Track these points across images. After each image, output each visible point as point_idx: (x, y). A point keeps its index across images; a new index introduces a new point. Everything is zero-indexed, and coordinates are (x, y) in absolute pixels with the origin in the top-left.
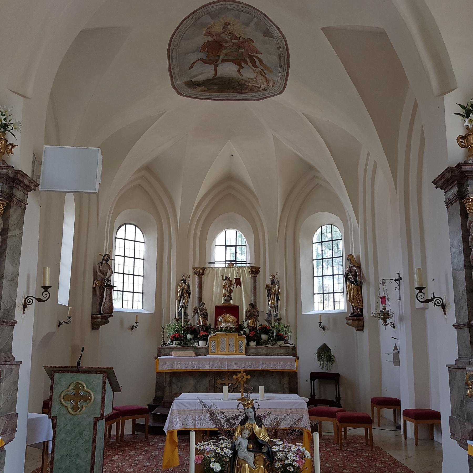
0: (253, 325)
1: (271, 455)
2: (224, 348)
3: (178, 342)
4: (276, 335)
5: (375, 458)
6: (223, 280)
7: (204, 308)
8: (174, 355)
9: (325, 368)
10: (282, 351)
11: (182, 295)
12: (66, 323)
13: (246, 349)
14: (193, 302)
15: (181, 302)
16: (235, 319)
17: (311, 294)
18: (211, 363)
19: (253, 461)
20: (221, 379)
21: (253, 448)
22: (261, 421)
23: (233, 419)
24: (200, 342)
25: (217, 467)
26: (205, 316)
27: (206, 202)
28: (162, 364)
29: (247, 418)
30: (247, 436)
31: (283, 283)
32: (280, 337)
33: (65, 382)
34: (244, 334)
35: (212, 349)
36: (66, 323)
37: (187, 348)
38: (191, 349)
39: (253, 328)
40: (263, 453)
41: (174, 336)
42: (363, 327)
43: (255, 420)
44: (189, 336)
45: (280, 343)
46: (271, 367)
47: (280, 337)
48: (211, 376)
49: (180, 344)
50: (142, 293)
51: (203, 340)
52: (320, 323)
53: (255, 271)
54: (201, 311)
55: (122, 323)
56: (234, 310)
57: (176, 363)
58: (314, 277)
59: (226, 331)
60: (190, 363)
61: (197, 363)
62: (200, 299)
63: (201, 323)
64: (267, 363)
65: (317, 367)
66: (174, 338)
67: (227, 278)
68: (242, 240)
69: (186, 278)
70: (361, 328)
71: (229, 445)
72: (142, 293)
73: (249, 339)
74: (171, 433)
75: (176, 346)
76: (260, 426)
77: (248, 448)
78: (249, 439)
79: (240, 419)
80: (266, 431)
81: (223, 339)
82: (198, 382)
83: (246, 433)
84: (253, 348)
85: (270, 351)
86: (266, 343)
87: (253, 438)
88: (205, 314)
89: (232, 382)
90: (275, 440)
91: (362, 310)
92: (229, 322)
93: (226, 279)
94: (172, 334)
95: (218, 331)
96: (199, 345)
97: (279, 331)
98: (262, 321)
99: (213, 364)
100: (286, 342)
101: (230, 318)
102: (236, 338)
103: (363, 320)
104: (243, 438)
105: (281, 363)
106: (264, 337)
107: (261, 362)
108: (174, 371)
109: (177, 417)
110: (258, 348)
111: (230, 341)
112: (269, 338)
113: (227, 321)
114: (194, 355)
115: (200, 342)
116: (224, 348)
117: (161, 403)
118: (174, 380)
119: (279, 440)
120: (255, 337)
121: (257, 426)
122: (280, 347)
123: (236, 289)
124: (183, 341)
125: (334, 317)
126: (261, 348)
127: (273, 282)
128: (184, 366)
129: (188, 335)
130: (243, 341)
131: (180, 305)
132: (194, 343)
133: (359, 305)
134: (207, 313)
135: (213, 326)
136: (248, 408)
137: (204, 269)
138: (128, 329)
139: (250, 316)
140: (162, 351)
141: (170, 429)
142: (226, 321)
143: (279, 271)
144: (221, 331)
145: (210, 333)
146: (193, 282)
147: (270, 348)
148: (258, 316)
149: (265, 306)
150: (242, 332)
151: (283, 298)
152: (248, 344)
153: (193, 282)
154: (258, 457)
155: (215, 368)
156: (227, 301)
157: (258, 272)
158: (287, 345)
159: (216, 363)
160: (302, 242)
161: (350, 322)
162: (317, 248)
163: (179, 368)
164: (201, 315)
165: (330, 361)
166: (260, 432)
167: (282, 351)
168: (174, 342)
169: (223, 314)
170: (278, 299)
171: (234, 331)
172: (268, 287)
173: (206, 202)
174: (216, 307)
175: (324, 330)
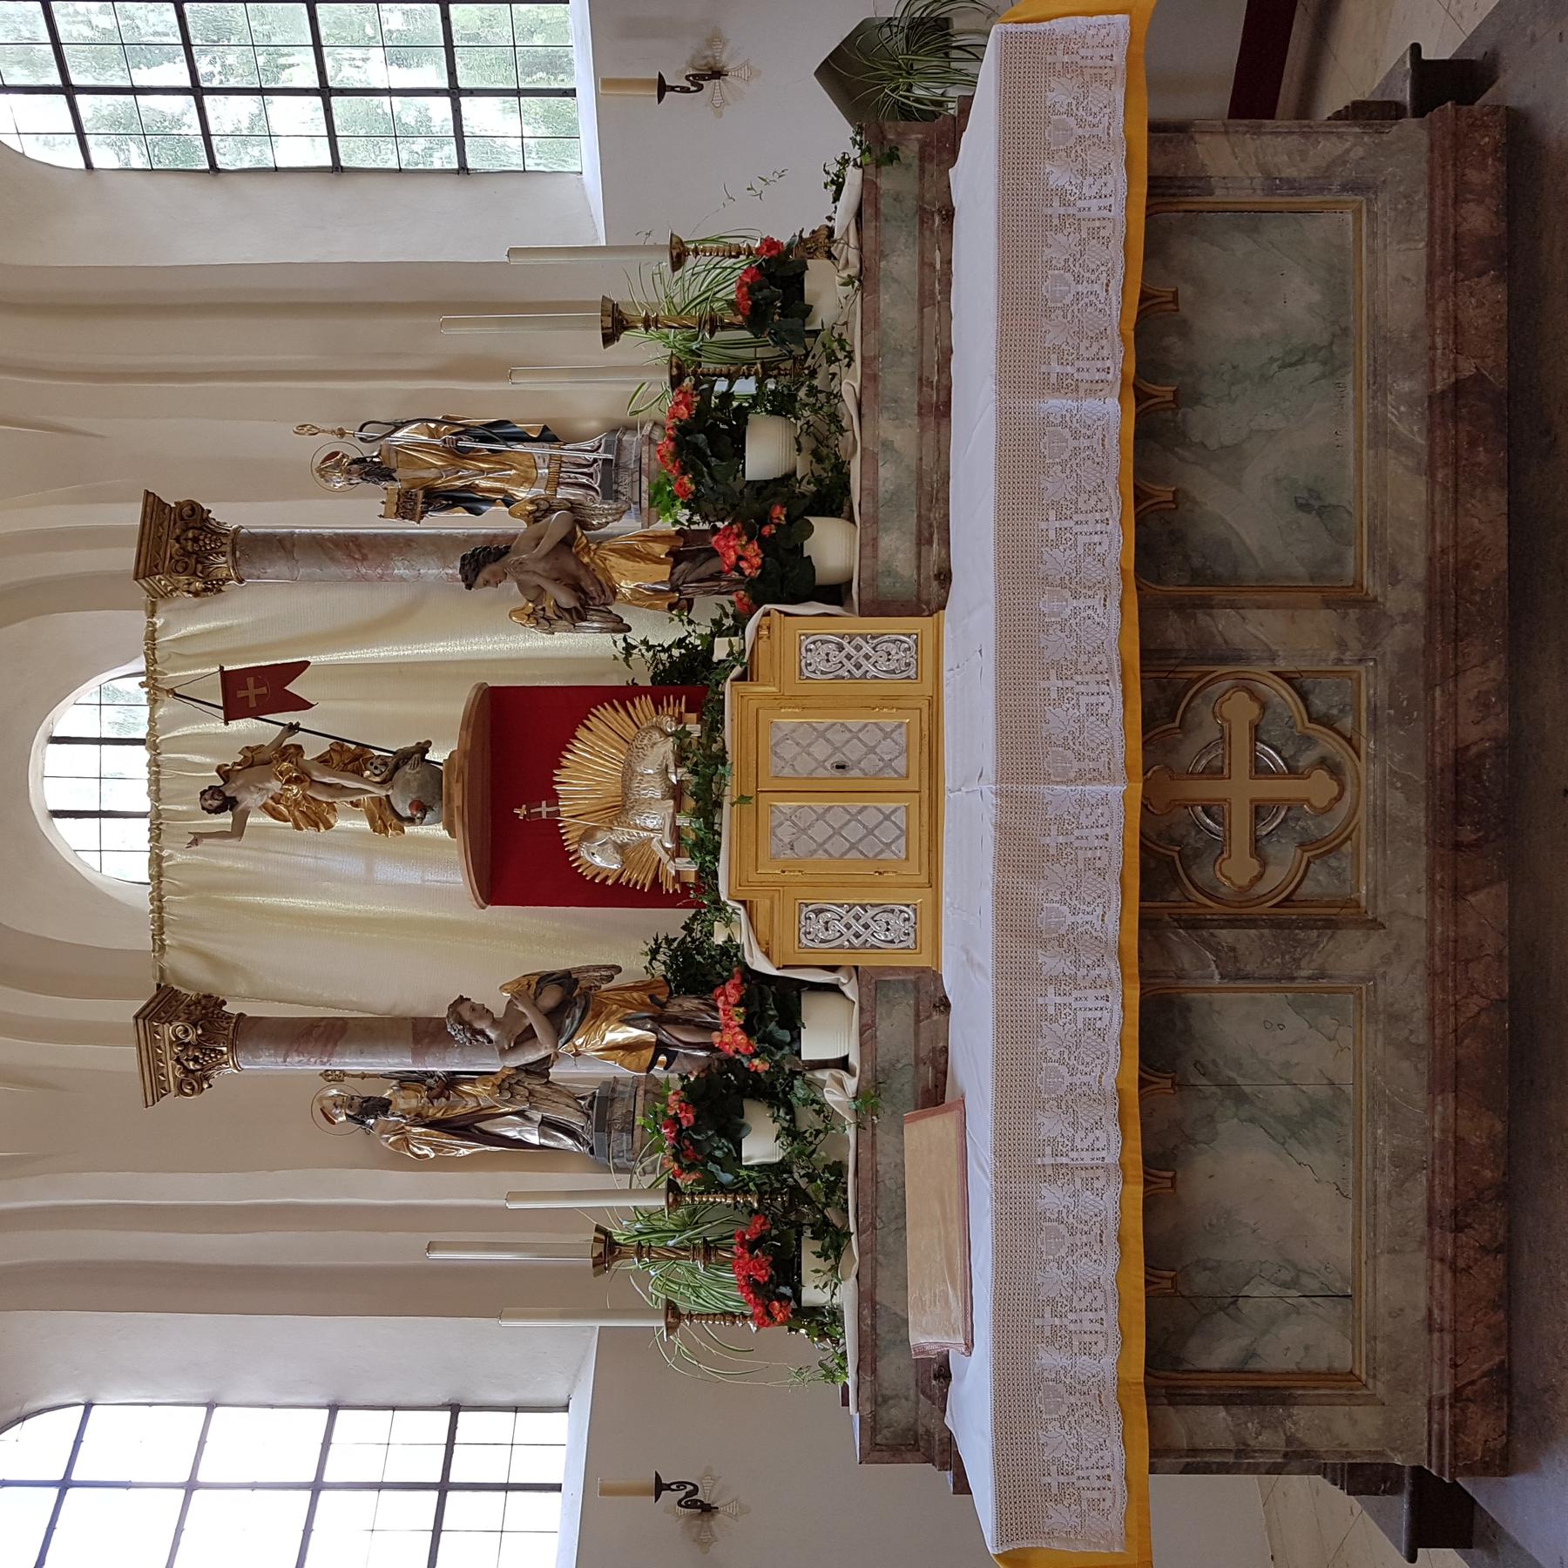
0: (660, 550)
2: (870, 818)
3: (809, 1262)
6: (238, 829)
7: (498, 1003)
10: (901, 264)
13: (879, 607)
15: (512, 1133)
16: (605, 720)
17: (454, 194)
18: (1053, 962)
20: (1218, 847)
24: (808, 1053)
26: (567, 999)
28: (1060, 1516)
31: (382, 397)
34: (738, 629)
35: (886, 938)
37: (872, 1180)
38: (883, 1138)
44: (761, 1145)
45: (827, 290)
48: (1186, 959)
49: (834, 1242)
50: (455, 1409)
51: (792, 1022)
52: (662, 88)
54: (527, 1037)
56: (519, 732)
58: (337, 168)
59: (708, 807)
60: (1052, 1197)
61: (1050, 1125)
63: (633, 1033)
64: (1054, 337)
66: (775, 1288)
67: (220, 799)
69: (349, 1102)
72: (455, 1409)
73: (788, 579)
81: (786, 833)
82: (1240, 1098)
84: (869, 545)
85: (899, 381)
86: (822, 445)
88: (550, 998)
89: (1241, 737)
92: (628, 773)
93: (228, 804)
95: (708, 875)
96: (843, 1064)
99: (1068, 942)
100: (822, 243)
101: (586, 772)
102: (780, 701)
105: (1058, 176)
106: (767, 451)
110: (870, 492)
111: (804, 766)
112: (782, 406)
113: (616, 793)
115: (808, 1053)
116: (870, 818)
117: (671, 735)
118: (1218, 1352)
120: (764, 519)
122: (864, 280)
123: (328, 716)
126: (870, 460)
127: (374, 471)
128: (1087, 1269)
130: (801, 636)
131: (534, 1139)
132: (822, 1109)
134: (545, 979)
135: (671, 921)
137: (165, 1003)
138: (704, 1543)
139: (576, 587)
140: (897, 1415)
142: (621, 808)
144: (706, 847)
145: (730, 952)
147: (870, 378)
150: (721, 650)
151: (483, 401)
152: (836, 593)
155: (1105, 911)
157: (193, 518)
159: (1057, 912)
167: (901, 264)
168: (812, 1295)
169: (552, 827)
170: (498, 432)
171: (714, 727)
175: (717, 74)
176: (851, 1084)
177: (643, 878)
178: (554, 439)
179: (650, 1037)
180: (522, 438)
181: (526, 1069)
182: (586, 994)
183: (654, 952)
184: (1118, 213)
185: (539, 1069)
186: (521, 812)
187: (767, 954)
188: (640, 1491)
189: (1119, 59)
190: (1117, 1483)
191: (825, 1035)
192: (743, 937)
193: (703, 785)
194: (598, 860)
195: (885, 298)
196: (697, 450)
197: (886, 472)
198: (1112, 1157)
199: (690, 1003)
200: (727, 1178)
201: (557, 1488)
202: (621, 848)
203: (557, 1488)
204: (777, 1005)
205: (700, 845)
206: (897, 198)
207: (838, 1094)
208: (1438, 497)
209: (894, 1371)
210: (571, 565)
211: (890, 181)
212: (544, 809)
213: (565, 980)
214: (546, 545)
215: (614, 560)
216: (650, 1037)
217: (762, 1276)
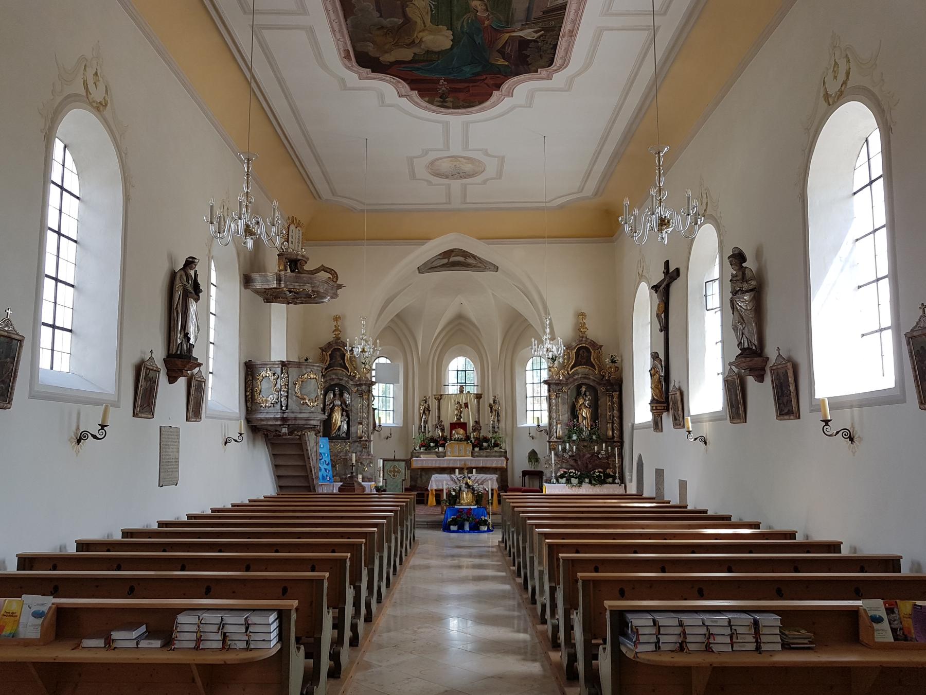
1: (473, 489)
8: (423, 457)
11: (424, 412)
12: (236, 441)
14: (432, 419)
25: (454, 493)
27: (442, 336)
31: (503, 402)
33: (389, 464)
35: (448, 453)
36: (236, 441)
39: (477, 439)
44: (432, 444)
45: (496, 449)
46: (488, 465)
47: (496, 445)
53: (478, 397)
56: (464, 426)
62: (439, 417)
65: (528, 467)
68: (471, 366)
73: (474, 446)
86: (486, 449)
87: (467, 484)
98: (484, 433)
101: (461, 431)
106: (485, 444)
107: (482, 462)
113: (459, 433)
123: (465, 411)
127: (494, 402)
129: (432, 444)
130: (470, 448)
143: (500, 393)
146: (433, 404)
149: (488, 420)
151: (503, 415)
153: (433, 404)
156: (459, 419)
160: (518, 369)
162: (529, 374)
170: (498, 415)
172: (490, 405)
173: (442, 336)
174: (451, 424)
191: (441, 449)
193: (459, 440)
201: (52, 368)
203: (52, 368)
208: (490, 549)
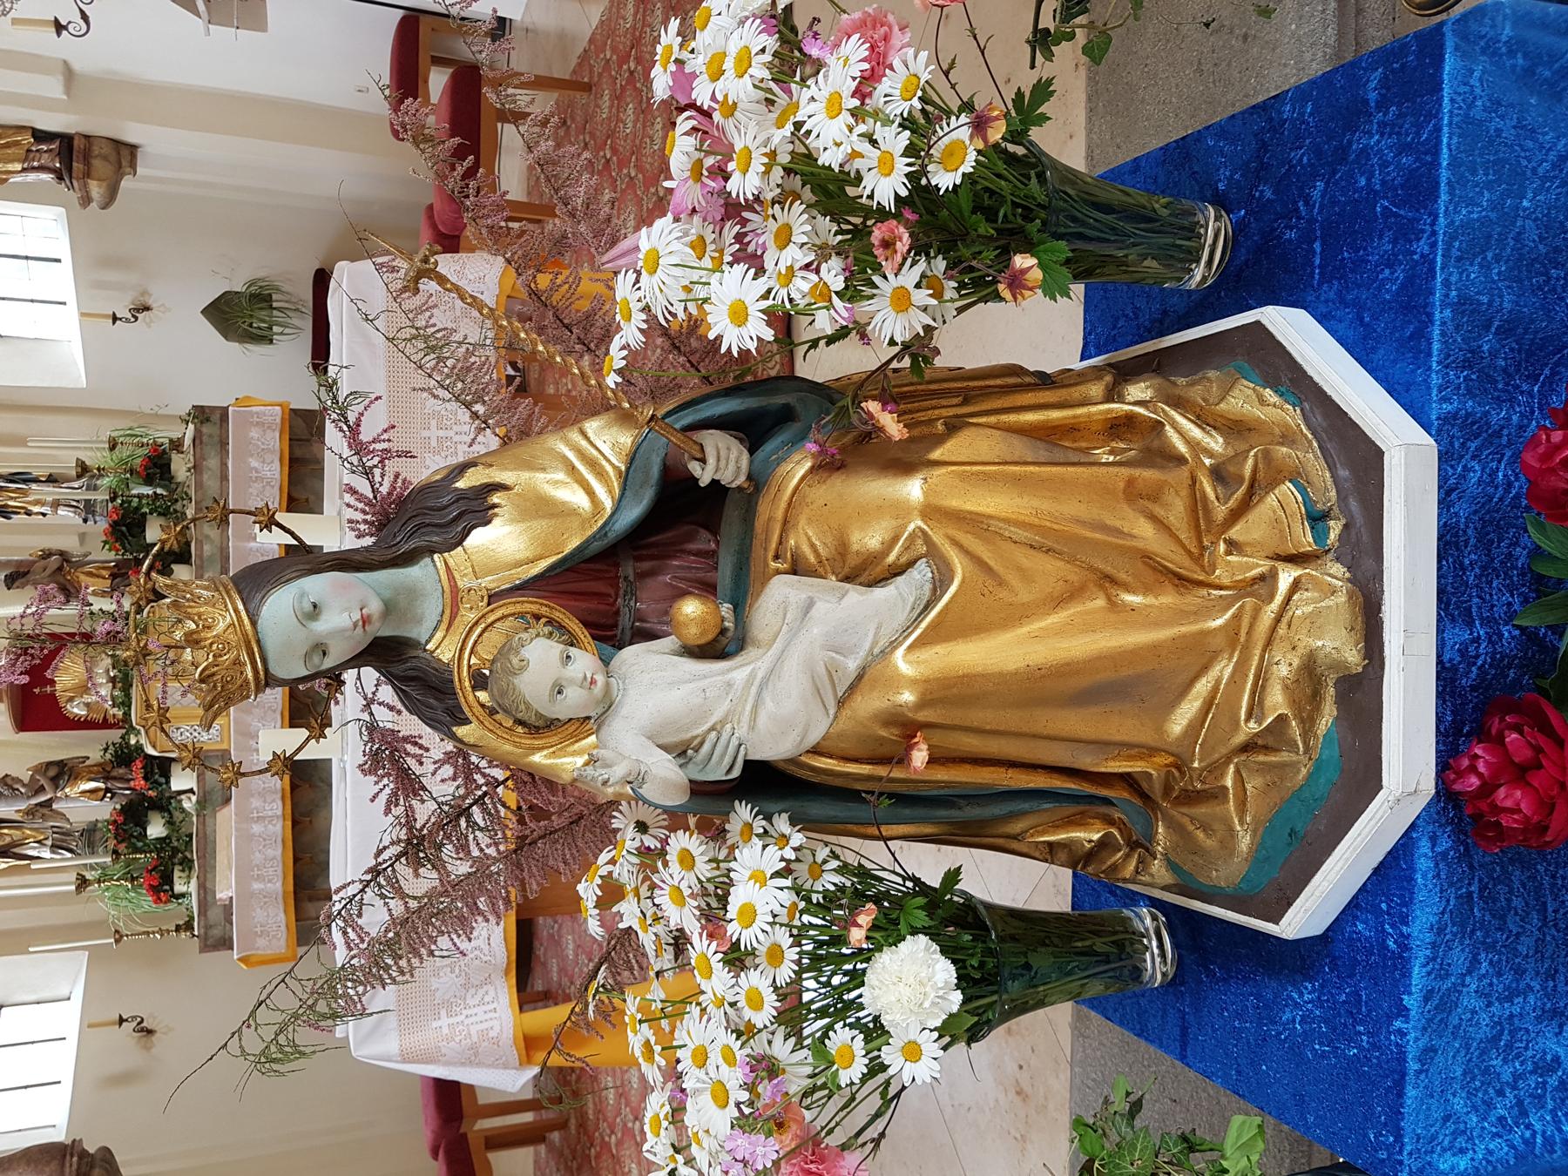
0: (106, 573)
3: (177, 874)
4: (149, 481)
5: (624, 59)
7: (26, 776)
9: (295, 321)
19: (855, 596)
21: (707, 589)
22: (427, 489)
23: (409, 785)
26: (62, 772)
29: (387, 652)
30: (584, 661)
32: (157, 466)
40: (757, 482)
41: (155, 891)
42: (117, 144)
43: (408, 559)
45: (180, 467)
47: (157, 466)
49: (187, 864)
51: (167, 775)
52: (115, 319)
54: (41, 789)
55: (123, 1079)
57: (256, 886)
59: (126, 689)
60: (257, 828)
66: (162, 887)
70: (124, 154)
71: (687, 860)
74: (530, 1044)
75: (194, 881)
76: (477, 508)
77: (717, 647)
78: (610, 634)
79: (410, 724)
80: (524, 450)
83: (549, 666)
87: (599, 591)
88: (52, 772)
90: (630, 334)
91: (40, 136)
94: (147, 902)
95: (127, 715)
96: (191, 791)
97: (132, 471)
100: (177, 445)
103: (87, 137)
104: (608, 705)
105: (254, 463)
106: (154, 532)
108: (291, 888)
109: (444, 1021)
110: (200, 556)
114: (225, 810)
119: (623, 286)
121: (478, 538)
122: (196, 468)
124: (175, 851)
125: (94, 262)
126: (200, 544)
128: (270, 852)
132: (183, 810)
133: (17, 143)
135: (115, 735)
136: (254, 644)
138: (148, 1048)
140: (216, 932)
141: (514, 1055)
144: (126, 704)
148: (62, 553)
154: (808, 538)
158: (188, 441)
161: (96, 189)
163: (280, 869)
164: (56, 787)
165: (268, 299)
166: (540, 508)
167: (213, 463)
168: (179, 888)
175: (147, 309)
176: (194, 798)
177: (99, 717)
178: (55, 481)
179: (102, 785)
180: (36, 480)
181: (40, 805)
182: (71, 769)
183: (106, 750)
184: (277, 476)
185: (47, 804)
186: (37, 691)
187: (154, 747)
188: (113, 1024)
189: (278, 420)
190: (283, 928)
191: (182, 780)
192: (143, 741)
194: (76, 710)
195: (205, 477)
196: (123, 534)
197: (206, 548)
198: (279, 812)
199: (122, 771)
200: (140, 844)
202: (87, 705)
204: (160, 768)
205: (123, 703)
206: (210, 436)
207: (189, 804)
209: (215, 914)
210: (62, 580)
211: (206, 429)
212: (49, 689)
213: (61, 764)
214: (48, 572)
215: (82, 577)
216: (102, 785)
217: (155, 883)
